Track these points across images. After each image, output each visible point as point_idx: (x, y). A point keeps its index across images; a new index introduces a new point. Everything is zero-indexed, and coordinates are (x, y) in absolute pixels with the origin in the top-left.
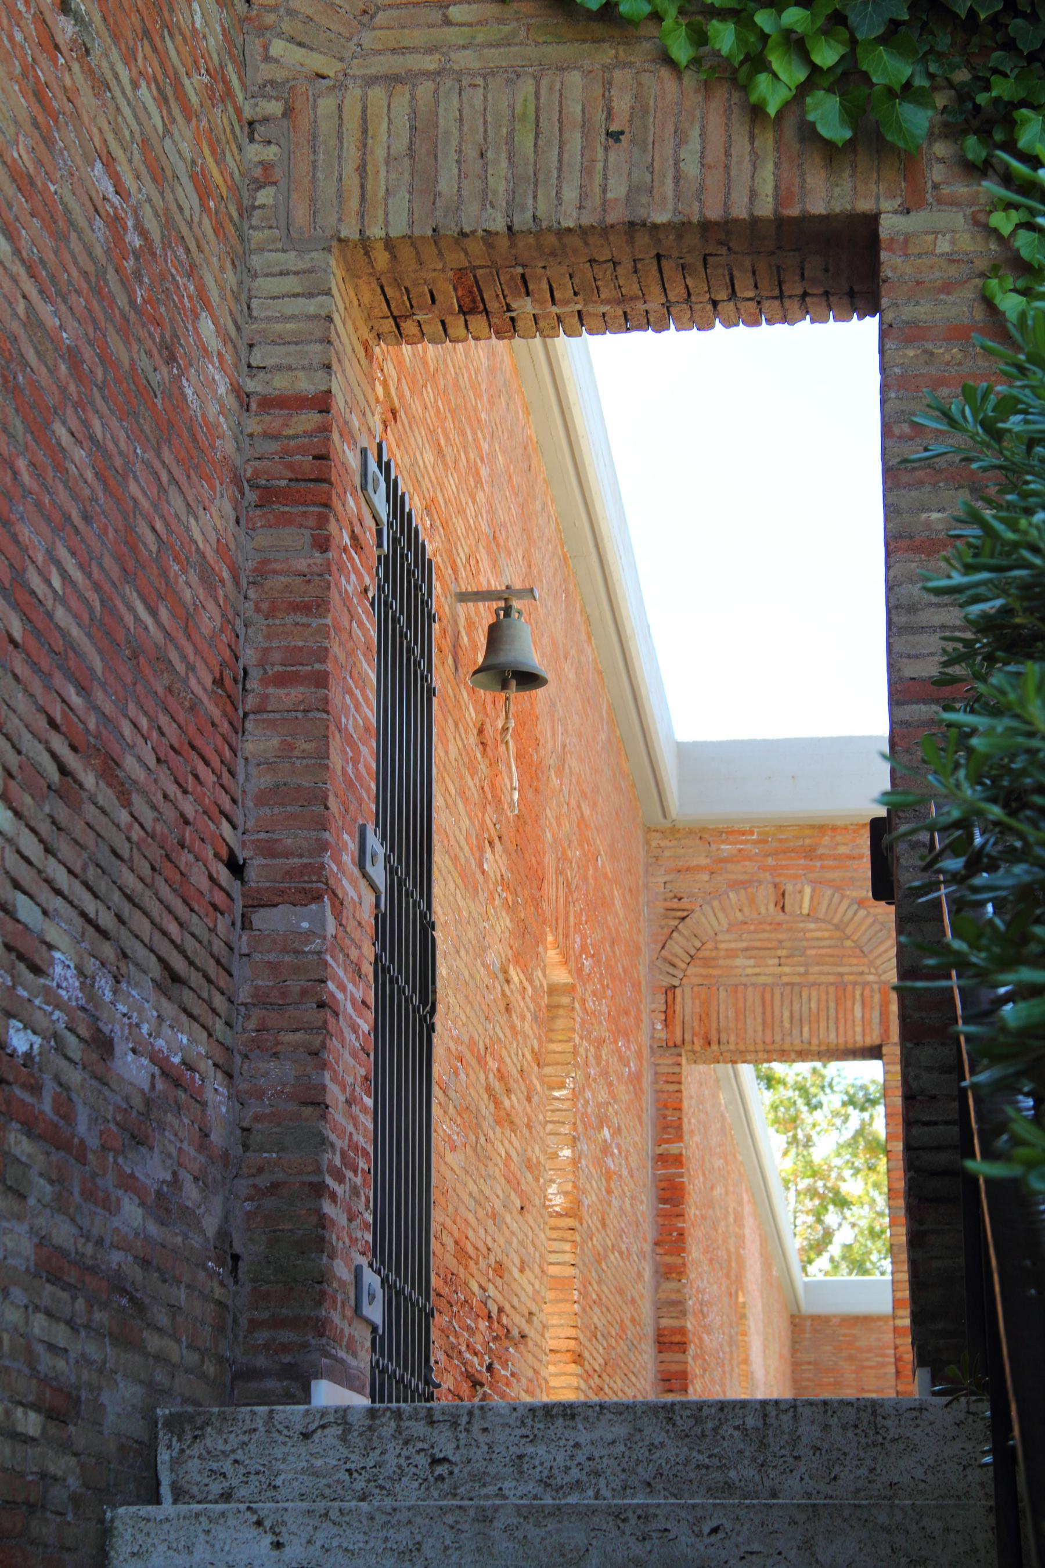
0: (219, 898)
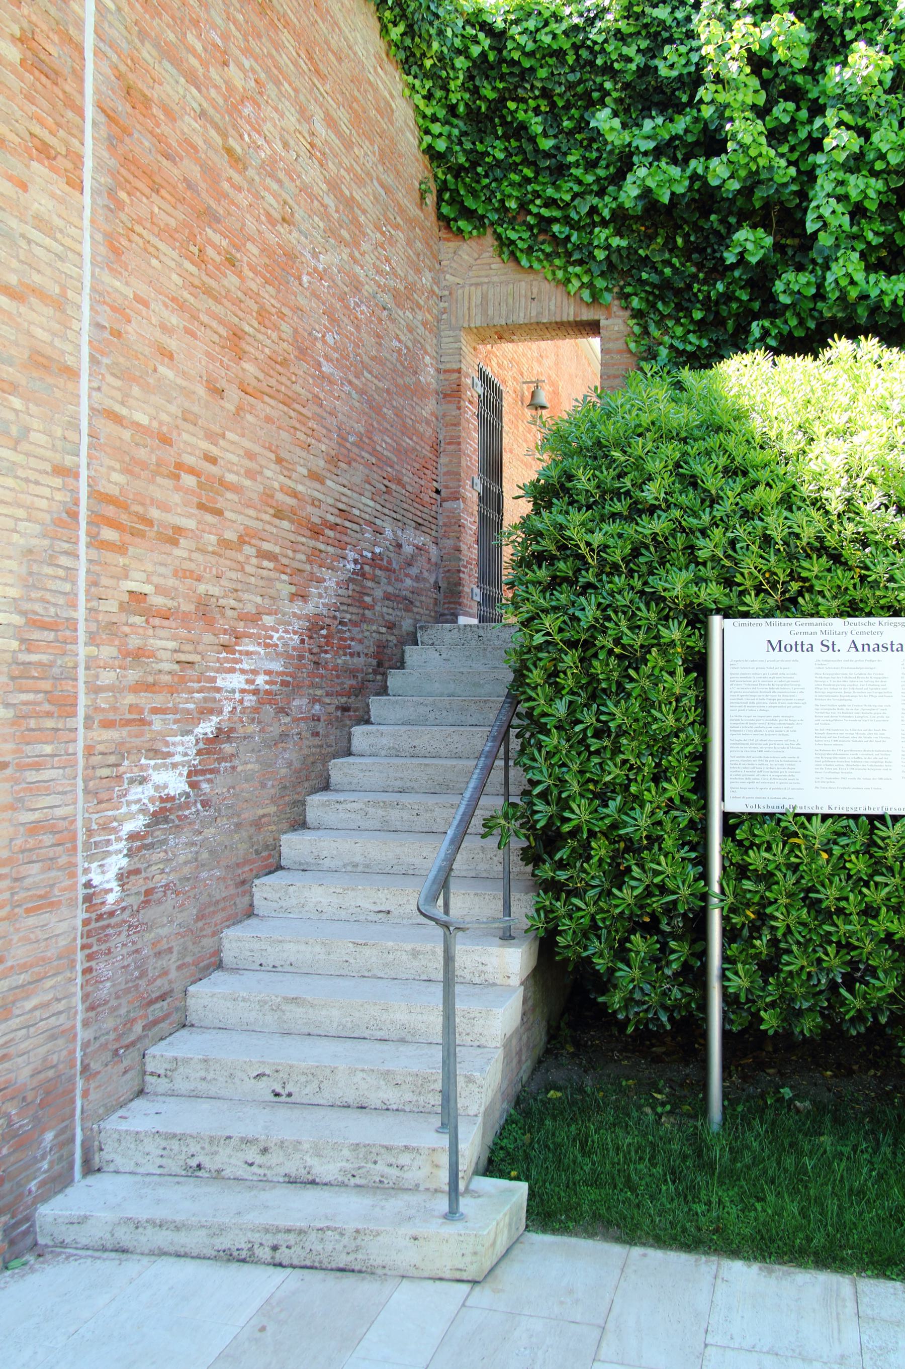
0: (433, 501)
